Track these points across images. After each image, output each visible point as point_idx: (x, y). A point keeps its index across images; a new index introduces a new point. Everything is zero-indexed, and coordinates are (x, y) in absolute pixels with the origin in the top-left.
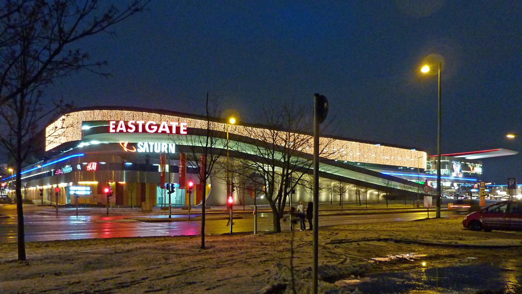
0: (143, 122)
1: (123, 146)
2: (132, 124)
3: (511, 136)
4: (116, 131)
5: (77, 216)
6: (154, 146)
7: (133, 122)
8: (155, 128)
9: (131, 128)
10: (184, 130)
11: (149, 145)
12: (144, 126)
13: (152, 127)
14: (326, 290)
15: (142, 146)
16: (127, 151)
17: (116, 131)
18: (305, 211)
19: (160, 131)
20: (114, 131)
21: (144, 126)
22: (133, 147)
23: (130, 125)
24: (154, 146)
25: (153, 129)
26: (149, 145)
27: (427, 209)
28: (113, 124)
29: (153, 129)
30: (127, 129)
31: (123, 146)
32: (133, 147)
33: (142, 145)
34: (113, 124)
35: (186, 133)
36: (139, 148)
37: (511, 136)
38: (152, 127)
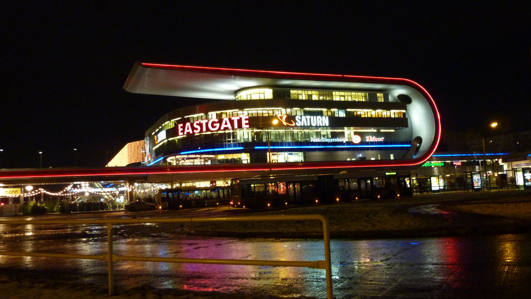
0: (206, 121)
1: (282, 120)
2: (197, 124)
3: (494, 125)
4: (184, 133)
5: (464, 191)
6: (310, 119)
7: (198, 122)
8: (218, 125)
9: (197, 129)
10: (246, 124)
11: (306, 119)
12: (207, 124)
13: (215, 125)
14: (167, 187)
15: (300, 120)
16: (286, 125)
17: (184, 133)
18: (485, 176)
19: (222, 128)
20: (182, 134)
21: (207, 124)
22: (292, 121)
23: (195, 126)
24: (310, 119)
25: (215, 127)
26: (306, 119)
27: (425, 177)
28: (181, 127)
29: (215, 127)
30: (193, 130)
31: (282, 120)
32: (292, 121)
33: (300, 118)
34: (181, 127)
35: (248, 126)
36: (297, 122)
37: (494, 125)
38: (215, 125)
